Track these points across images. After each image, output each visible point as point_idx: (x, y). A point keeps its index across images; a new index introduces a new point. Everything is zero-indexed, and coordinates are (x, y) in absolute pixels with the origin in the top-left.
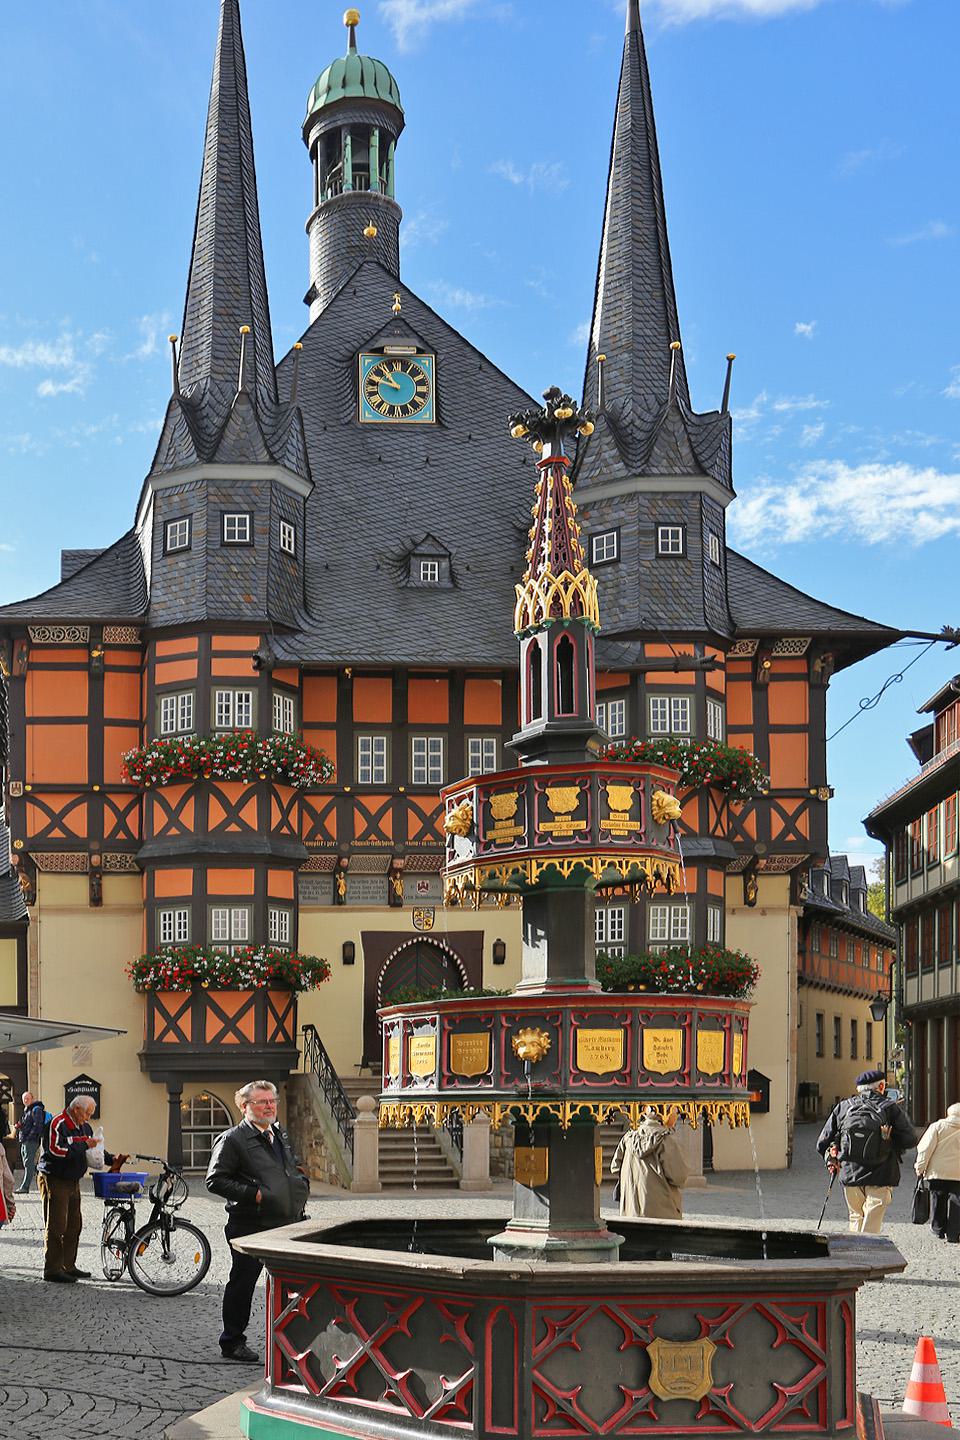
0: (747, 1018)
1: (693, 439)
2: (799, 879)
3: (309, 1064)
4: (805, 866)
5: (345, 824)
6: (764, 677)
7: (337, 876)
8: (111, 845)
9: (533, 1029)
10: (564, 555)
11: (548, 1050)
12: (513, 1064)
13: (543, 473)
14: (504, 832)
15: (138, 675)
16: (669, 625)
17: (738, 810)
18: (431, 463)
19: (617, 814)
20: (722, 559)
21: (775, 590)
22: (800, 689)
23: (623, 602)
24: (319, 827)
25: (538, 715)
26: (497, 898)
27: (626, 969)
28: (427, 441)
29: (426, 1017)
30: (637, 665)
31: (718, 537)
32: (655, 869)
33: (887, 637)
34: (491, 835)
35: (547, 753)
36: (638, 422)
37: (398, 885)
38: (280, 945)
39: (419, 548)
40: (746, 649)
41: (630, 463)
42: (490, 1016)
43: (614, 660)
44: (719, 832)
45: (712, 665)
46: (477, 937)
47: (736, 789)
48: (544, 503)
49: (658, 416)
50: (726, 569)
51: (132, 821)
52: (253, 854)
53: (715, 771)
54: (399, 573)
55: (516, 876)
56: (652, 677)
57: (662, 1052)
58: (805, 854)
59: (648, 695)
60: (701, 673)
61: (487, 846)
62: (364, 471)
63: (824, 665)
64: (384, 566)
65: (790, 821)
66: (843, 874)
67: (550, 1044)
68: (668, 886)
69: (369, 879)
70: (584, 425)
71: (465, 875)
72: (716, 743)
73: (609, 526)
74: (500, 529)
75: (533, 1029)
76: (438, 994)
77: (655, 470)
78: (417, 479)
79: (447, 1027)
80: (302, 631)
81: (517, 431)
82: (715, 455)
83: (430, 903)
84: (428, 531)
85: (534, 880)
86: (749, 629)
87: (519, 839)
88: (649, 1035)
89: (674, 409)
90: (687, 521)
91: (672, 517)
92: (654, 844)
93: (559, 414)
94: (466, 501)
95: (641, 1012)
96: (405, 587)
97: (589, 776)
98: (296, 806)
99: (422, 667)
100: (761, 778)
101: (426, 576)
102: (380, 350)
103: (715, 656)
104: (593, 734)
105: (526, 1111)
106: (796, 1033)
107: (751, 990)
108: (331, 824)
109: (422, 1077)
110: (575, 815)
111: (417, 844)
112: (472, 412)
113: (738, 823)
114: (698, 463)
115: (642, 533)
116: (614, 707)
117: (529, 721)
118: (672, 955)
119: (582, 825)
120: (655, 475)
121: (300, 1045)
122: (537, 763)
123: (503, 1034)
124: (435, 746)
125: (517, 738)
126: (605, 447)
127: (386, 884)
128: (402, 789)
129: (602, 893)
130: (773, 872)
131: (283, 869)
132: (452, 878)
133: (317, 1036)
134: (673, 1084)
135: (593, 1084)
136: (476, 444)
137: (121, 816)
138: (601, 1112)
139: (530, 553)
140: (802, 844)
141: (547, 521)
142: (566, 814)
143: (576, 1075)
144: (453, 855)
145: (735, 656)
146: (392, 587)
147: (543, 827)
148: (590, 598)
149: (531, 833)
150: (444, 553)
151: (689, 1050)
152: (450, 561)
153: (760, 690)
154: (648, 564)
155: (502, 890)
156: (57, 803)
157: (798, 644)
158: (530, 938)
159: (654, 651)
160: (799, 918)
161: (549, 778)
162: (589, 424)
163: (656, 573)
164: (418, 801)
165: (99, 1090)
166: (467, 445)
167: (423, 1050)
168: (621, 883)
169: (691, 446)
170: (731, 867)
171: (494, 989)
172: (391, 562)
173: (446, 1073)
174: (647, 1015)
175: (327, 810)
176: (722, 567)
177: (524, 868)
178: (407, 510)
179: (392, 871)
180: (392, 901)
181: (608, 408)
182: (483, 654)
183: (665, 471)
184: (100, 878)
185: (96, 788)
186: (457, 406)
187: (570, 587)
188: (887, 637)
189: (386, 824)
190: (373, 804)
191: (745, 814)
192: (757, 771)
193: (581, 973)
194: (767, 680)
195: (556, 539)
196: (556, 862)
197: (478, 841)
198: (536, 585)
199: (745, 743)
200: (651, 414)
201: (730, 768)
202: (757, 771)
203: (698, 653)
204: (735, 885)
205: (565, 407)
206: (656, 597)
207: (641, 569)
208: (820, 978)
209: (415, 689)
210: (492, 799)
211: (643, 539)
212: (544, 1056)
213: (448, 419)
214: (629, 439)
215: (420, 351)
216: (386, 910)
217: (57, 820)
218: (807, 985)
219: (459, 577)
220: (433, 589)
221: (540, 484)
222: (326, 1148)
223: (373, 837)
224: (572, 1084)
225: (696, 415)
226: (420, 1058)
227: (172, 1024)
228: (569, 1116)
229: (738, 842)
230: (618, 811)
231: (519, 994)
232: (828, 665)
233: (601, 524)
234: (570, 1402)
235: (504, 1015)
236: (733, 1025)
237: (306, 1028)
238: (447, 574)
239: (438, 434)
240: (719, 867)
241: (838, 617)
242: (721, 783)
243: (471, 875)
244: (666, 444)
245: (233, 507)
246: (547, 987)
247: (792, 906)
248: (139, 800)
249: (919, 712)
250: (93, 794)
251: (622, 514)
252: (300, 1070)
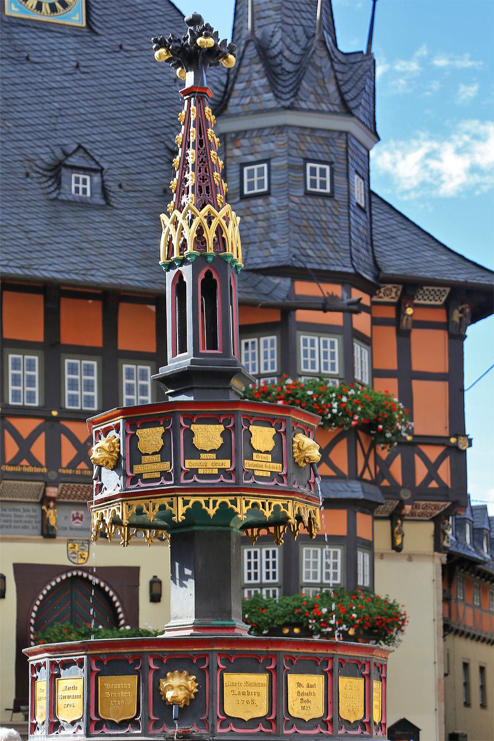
0: (386, 665)
1: (339, 76)
2: (442, 526)
4: (446, 514)
6: (407, 323)
9: (181, 672)
10: (207, 188)
11: (195, 694)
13: (186, 101)
14: (151, 467)
16: (318, 264)
17: (384, 454)
18: (83, 69)
19: (260, 454)
20: (367, 202)
21: (416, 237)
22: (440, 337)
23: (274, 236)
25: (183, 349)
26: (145, 534)
27: (280, 611)
28: (78, 46)
29: (73, 658)
30: (287, 301)
31: (363, 179)
32: (296, 512)
34: (138, 469)
35: (192, 388)
36: (287, 53)
39: (70, 159)
40: (390, 294)
41: (279, 94)
42: (137, 658)
43: (266, 295)
44: (367, 476)
45: (357, 307)
46: (133, 573)
47: (382, 433)
48: (188, 133)
49: (306, 49)
50: (370, 212)
52: (305, 269)
53: (362, 414)
54: (50, 183)
55: (162, 513)
56: (302, 315)
58: (447, 501)
59: (298, 333)
60: (348, 314)
61: (134, 480)
62: (11, 68)
64: (34, 175)
65: (433, 468)
66: (483, 523)
67: (197, 687)
68: (309, 528)
69: (20, 507)
70: (226, 57)
71: (112, 509)
72: (363, 385)
73: (259, 157)
74: (152, 148)
75: (181, 672)
76: (87, 635)
77: (303, 105)
78: (67, 84)
79: (95, 669)
81: (160, 54)
82: (360, 96)
83: (83, 535)
84: (79, 141)
85: (180, 518)
86: (393, 274)
87: (165, 475)
88: (293, 680)
89: (321, 43)
90: (334, 160)
91: (320, 155)
92: (295, 486)
93: (201, 42)
94: (118, 115)
95: (285, 656)
96: (56, 199)
97: (233, 414)
99: (75, 286)
100: (405, 424)
101: (77, 189)
103: (360, 299)
104: (236, 372)
106: (442, 681)
107: (400, 636)
109: (69, 721)
110: (221, 453)
111: (70, 472)
112: (123, 20)
113: (384, 466)
114: (344, 102)
115: (291, 167)
116: (265, 343)
117: (174, 355)
118: (325, 598)
119: (226, 464)
120: (303, 110)
122: (183, 398)
123: (151, 677)
124: (89, 370)
125: (164, 371)
126: (255, 75)
127: (38, 514)
128: (55, 413)
129: (247, 534)
130: (417, 518)
132: (99, 512)
134: (316, 732)
135: (240, 731)
136: (127, 55)
139: (174, 183)
140: (443, 492)
141: (191, 151)
142: (212, 451)
143: (98, 722)
144: (100, 488)
146: (42, 197)
147: (189, 464)
148: (232, 234)
149: (177, 469)
150: (95, 167)
151: (331, 697)
152: (102, 176)
153: (403, 335)
154: (296, 200)
155: (150, 527)
157: (438, 293)
158: (177, 576)
159: (304, 289)
160: (443, 566)
161: (195, 414)
162: (231, 57)
163: (305, 210)
164: (72, 426)
166: (118, 55)
167: (71, 693)
168: (265, 525)
169: (337, 84)
170: (380, 511)
171: (150, 628)
172: (41, 171)
173: (94, 718)
174: (291, 659)
175: (34, 435)
176: (367, 210)
177: (171, 505)
178: (57, 117)
179: (45, 500)
180: (45, 532)
181: (258, 34)
182: (137, 278)
183: (312, 106)
186: (107, 12)
187: (213, 221)
189: (39, 449)
190: (25, 426)
191: (390, 459)
192: (401, 417)
193: (228, 614)
194: (409, 327)
195: (200, 171)
196: (202, 500)
197: (125, 475)
198: (180, 216)
199: (389, 388)
200: (299, 45)
201: (376, 412)
202: (401, 417)
203: (345, 295)
204: (383, 529)
205: (207, 36)
206: (305, 234)
207: (291, 205)
208: (465, 626)
209: (68, 310)
210: (139, 432)
211: (292, 174)
212: (191, 700)
213: (99, 24)
214: (278, 70)
216: (36, 541)
218: (453, 633)
219: (111, 194)
220: (83, 205)
221: (183, 112)
223: (25, 462)
224: (219, 731)
225: (342, 53)
226: (67, 701)
229: (386, 487)
230: (261, 452)
231: (167, 635)
232: (465, 316)
233: (252, 154)
235: (151, 656)
236: (372, 671)
238: (99, 190)
239: (88, 39)
240: (368, 511)
241: (474, 269)
242: (368, 426)
243: (121, 511)
244: (314, 79)
246: (195, 628)
247: (436, 553)
251: (272, 146)
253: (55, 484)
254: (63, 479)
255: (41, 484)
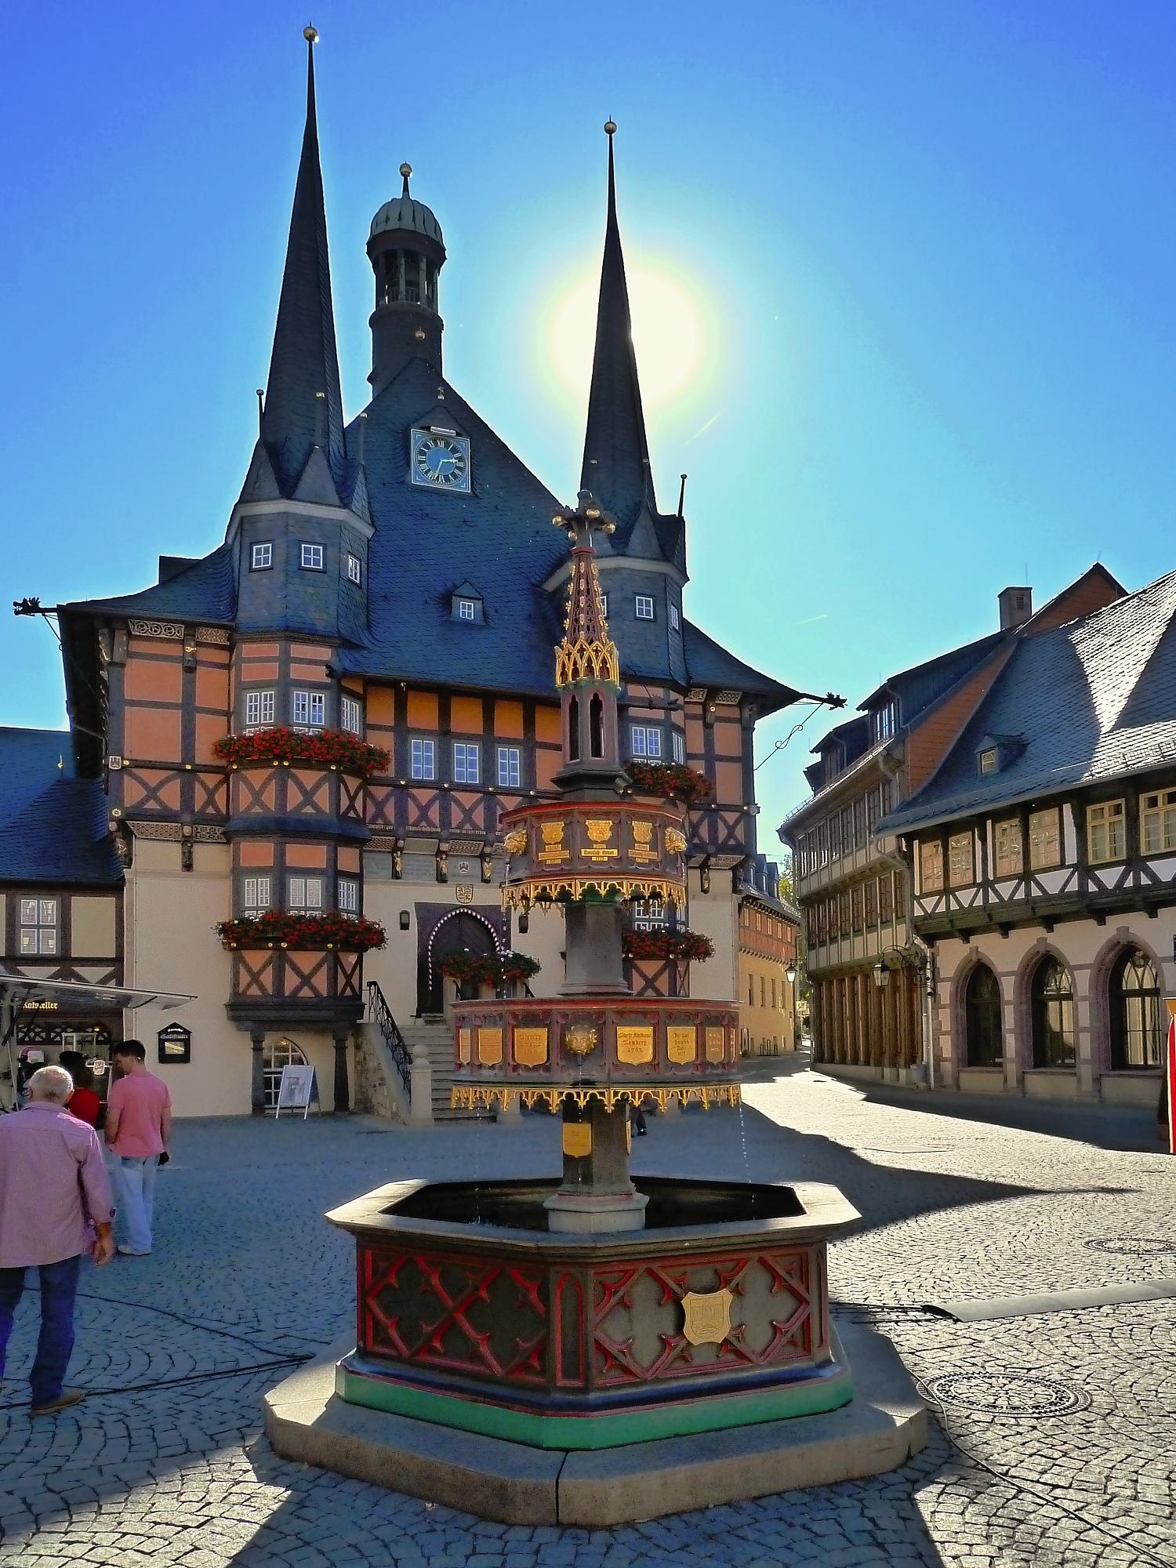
3: (373, 1015)
4: (742, 864)
5: (401, 812)
7: (395, 855)
8: (201, 819)
10: (594, 627)
12: (570, 1056)
15: (227, 671)
22: (735, 728)
24: (380, 813)
33: (789, 697)
37: (443, 864)
38: (348, 912)
40: (698, 696)
51: (220, 798)
57: (681, 1046)
63: (751, 713)
65: (731, 829)
67: (596, 1039)
69: (421, 858)
80: (365, 648)
98: (361, 794)
101: (464, 613)
102: (428, 429)
105: (579, 1097)
108: (390, 811)
110: (609, 844)
119: (615, 852)
121: (365, 998)
124: (472, 752)
128: (446, 786)
131: (352, 847)
133: (379, 992)
137: (211, 793)
138: (637, 1098)
142: (602, 842)
145: (691, 700)
150: (479, 596)
153: (708, 726)
156: (153, 777)
157: (733, 696)
165: (189, 1037)
175: (431, 802)
184: (192, 846)
185: (188, 767)
188: (789, 697)
189: (434, 813)
190: (424, 795)
215: (458, 434)
216: (431, 886)
217: (152, 793)
220: (468, 625)
222: (388, 1089)
223: (424, 824)
227: (255, 978)
228: (613, 1101)
234: (624, 1354)
237: (370, 984)
245: (308, 539)
248: (226, 780)
249: (812, 752)
250: (186, 772)
252: (365, 1020)
253: (447, 841)
254: (454, 837)
255: (436, 840)
